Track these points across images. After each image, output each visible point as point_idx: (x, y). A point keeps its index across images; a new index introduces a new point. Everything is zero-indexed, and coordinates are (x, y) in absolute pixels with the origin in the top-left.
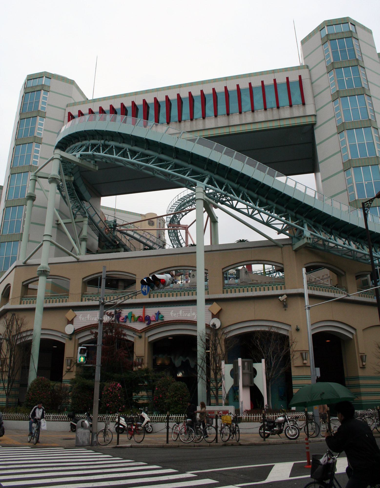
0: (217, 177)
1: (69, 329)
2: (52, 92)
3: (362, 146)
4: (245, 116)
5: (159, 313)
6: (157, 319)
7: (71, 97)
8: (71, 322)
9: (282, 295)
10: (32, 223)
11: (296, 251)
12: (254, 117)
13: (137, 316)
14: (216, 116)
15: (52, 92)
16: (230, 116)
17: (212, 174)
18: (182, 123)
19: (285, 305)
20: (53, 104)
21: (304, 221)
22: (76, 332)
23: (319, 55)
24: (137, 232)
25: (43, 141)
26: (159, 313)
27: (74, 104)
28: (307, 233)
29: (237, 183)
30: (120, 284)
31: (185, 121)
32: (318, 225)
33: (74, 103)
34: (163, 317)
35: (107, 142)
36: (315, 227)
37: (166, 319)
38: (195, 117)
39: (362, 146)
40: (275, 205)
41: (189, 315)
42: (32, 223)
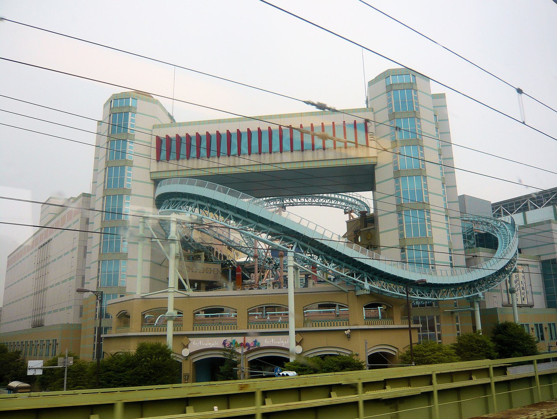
0: (302, 243)
1: (186, 352)
2: (139, 113)
3: (412, 192)
4: (317, 153)
5: (256, 341)
6: (255, 345)
7: (156, 118)
8: (187, 347)
9: (346, 330)
10: (144, 260)
11: (358, 296)
12: (324, 155)
13: (239, 343)
14: (292, 151)
15: (139, 113)
16: (304, 152)
17: (299, 242)
18: (262, 155)
19: (348, 337)
20: (143, 130)
21: (365, 275)
22: (191, 354)
23: (382, 102)
24: (221, 243)
25: (134, 164)
26: (256, 341)
27: (159, 126)
28: (367, 285)
29: (317, 248)
30: (203, 285)
31: (264, 153)
32: (375, 277)
33: (160, 125)
34: (259, 344)
35: (213, 206)
36: (372, 279)
37: (262, 345)
38: (273, 150)
39: (412, 192)
40: (344, 264)
41: (279, 343)
42: (144, 260)
